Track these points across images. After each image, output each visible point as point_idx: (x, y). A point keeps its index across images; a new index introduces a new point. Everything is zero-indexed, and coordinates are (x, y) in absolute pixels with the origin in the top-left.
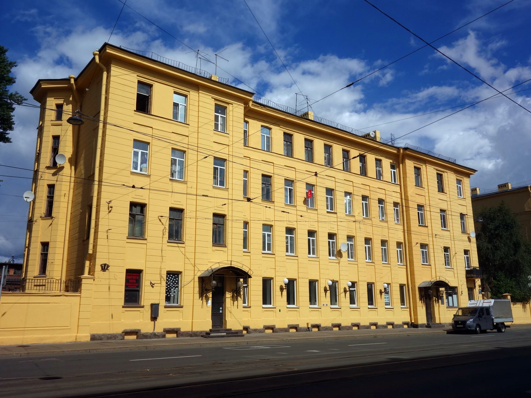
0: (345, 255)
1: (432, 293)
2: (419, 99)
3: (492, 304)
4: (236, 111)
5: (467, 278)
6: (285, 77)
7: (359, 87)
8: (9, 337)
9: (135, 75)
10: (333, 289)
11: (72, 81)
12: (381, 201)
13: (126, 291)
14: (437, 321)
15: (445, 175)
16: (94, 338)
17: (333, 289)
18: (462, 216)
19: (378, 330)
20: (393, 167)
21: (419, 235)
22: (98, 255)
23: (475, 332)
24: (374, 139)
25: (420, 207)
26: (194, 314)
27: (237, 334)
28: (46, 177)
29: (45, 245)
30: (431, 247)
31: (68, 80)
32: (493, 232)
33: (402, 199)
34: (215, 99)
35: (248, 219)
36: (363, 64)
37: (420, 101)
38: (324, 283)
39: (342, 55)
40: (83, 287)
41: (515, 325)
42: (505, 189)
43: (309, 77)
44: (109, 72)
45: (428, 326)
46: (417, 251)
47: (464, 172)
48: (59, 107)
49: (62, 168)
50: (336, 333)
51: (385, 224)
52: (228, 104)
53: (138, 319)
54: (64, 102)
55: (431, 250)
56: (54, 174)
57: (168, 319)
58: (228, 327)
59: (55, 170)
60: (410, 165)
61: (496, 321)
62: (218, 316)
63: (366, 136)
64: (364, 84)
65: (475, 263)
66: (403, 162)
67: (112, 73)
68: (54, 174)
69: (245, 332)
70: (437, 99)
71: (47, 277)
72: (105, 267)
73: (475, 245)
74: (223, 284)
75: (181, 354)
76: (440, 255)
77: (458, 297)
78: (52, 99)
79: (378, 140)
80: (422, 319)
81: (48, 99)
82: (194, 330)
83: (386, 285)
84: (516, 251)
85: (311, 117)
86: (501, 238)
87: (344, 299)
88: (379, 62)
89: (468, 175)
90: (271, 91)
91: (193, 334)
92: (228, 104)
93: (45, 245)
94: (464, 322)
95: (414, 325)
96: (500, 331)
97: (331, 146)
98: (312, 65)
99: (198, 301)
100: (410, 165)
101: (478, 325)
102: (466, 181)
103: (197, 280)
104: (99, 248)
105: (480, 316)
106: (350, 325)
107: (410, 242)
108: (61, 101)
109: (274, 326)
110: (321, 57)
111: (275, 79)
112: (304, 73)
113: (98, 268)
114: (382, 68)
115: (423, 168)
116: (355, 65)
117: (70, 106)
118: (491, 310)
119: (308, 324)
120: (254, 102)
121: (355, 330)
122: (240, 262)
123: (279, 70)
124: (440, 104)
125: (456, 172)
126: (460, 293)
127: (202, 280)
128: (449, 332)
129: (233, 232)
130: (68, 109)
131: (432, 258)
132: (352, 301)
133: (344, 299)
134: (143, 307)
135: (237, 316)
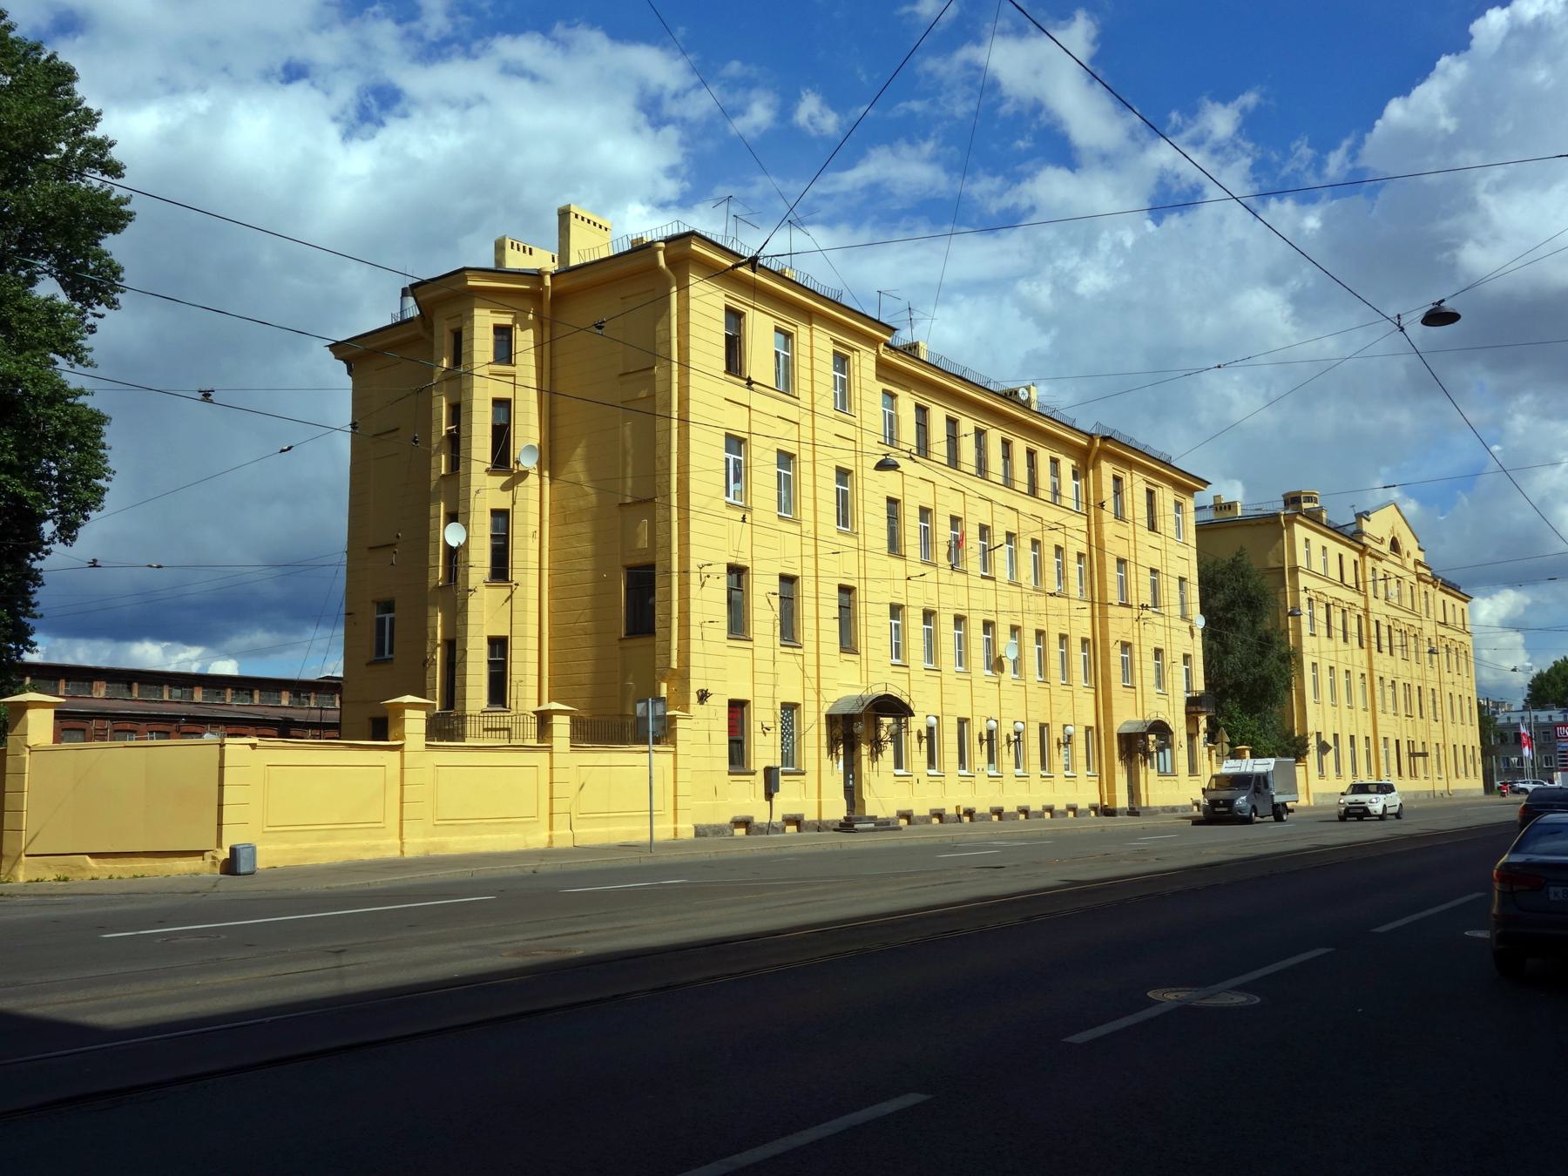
0: (1008, 666)
1: (1138, 745)
2: (842, 187)
3: (1271, 768)
4: (864, 362)
5: (1187, 713)
6: (455, 76)
7: (671, 133)
8: (436, 839)
9: (722, 294)
10: (990, 738)
11: (548, 281)
12: (1058, 549)
13: (730, 741)
14: (1144, 804)
15: (1158, 492)
16: (700, 832)
17: (990, 738)
18: (1182, 580)
19: (805, 834)
20: (1075, 476)
21: (1120, 625)
22: (693, 672)
23: (1247, 821)
24: (1025, 406)
25: (1121, 562)
26: (816, 792)
27: (884, 825)
28: (485, 491)
29: (499, 646)
30: (1136, 648)
31: (538, 275)
32: (1221, 614)
33: (1090, 545)
34: (836, 342)
35: (932, 606)
36: (680, 65)
37: (847, 195)
38: (978, 727)
39: (622, 32)
40: (680, 734)
41: (1302, 809)
42: (1229, 514)
43: (523, 85)
44: (684, 287)
45: (1133, 812)
46: (1116, 655)
47: (1187, 484)
48: (503, 333)
49: (525, 474)
50: (791, 838)
51: (990, 584)
52: (852, 350)
53: (746, 798)
54: (515, 320)
55: (1137, 656)
56: (504, 488)
57: (793, 798)
58: (869, 812)
59: (506, 478)
60: (1107, 469)
61: (1278, 799)
62: (852, 793)
63: (1010, 396)
64: (683, 123)
65: (1199, 685)
66: (1096, 466)
67: (693, 291)
68: (504, 488)
69: (903, 822)
70: (891, 194)
71: (513, 712)
72: (703, 696)
73: (1200, 645)
74: (861, 728)
75: (162, 923)
76: (1150, 664)
77: (1172, 754)
78: (487, 312)
79: (1034, 407)
80: (1122, 801)
81: (477, 312)
82: (825, 817)
83: (933, 721)
84: (1263, 654)
85: (923, 356)
86: (1238, 628)
87: (1006, 757)
88: (735, 68)
89: (1190, 491)
90: (405, 115)
91: (820, 826)
92: (852, 350)
93: (499, 646)
94: (1229, 803)
95: (1108, 812)
96: (1279, 819)
97: (984, 432)
98: (525, 49)
99: (826, 762)
100: (1107, 469)
101: (1254, 808)
102: (1189, 504)
103: (823, 720)
104: (694, 660)
105: (1257, 790)
106: (927, 813)
107: (1105, 640)
108: (506, 320)
109: (802, 816)
110: (559, 30)
111: (416, 81)
112: (513, 70)
113: (694, 698)
114: (748, 84)
115: (1127, 477)
116: (656, 66)
117: (530, 333)
118: (1270, 779)
119: (958, 808)
120: (887, 345)
121: (739, 839)
122: (897, 686)
123: (433, 51)
124: (898, 207)
125: (1178, 486)
126: (1176, 745)
127: (832, 719)
128: (1197, 822)
129: (874, 626)
130: (524, 340)
131: (1138, 673)
132: (931, 762)
133: (1006, 757)
134: (753, 773)
135: (887, 790)
